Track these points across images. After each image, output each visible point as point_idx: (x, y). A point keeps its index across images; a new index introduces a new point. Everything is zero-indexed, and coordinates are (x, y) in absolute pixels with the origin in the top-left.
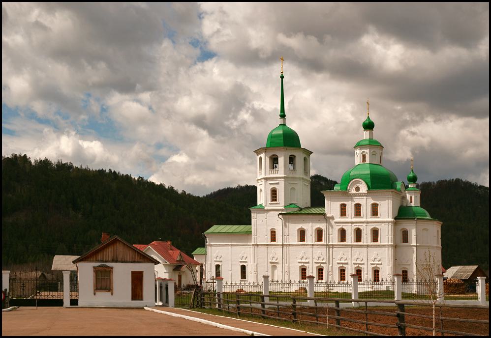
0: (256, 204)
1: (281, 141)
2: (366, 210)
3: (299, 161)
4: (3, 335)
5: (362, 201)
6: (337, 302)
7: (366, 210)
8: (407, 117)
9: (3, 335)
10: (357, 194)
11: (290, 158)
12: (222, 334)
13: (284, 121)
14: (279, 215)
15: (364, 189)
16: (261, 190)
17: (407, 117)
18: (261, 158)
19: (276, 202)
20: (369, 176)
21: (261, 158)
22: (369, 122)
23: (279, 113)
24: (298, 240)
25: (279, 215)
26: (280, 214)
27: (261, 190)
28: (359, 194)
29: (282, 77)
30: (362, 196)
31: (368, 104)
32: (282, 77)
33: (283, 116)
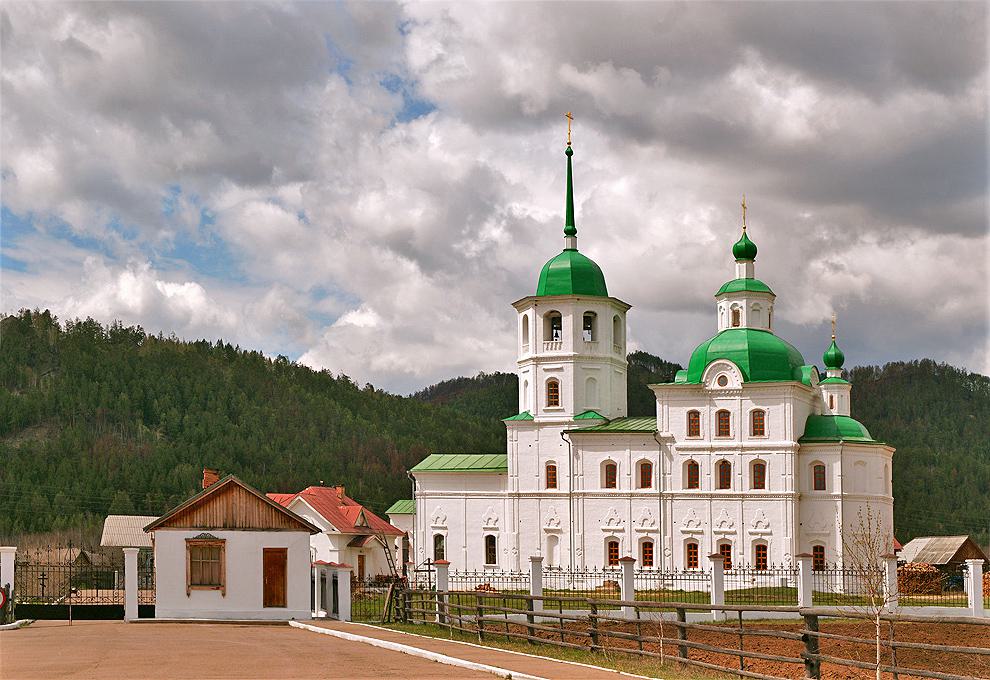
0: (517, 412)
2: (740, 423)
3: (604, 323)
7: (740, 423)
10: (721, 390)
13: (574, 243)
14: (562, 434)
15: (735, 380)
16: (526, 383)
19: (556, 408)
21: (526, 317)
24: (750, 485)
25: (562, 434)
29: (569, 153)
32: (569, 153)
33: (571, 232)
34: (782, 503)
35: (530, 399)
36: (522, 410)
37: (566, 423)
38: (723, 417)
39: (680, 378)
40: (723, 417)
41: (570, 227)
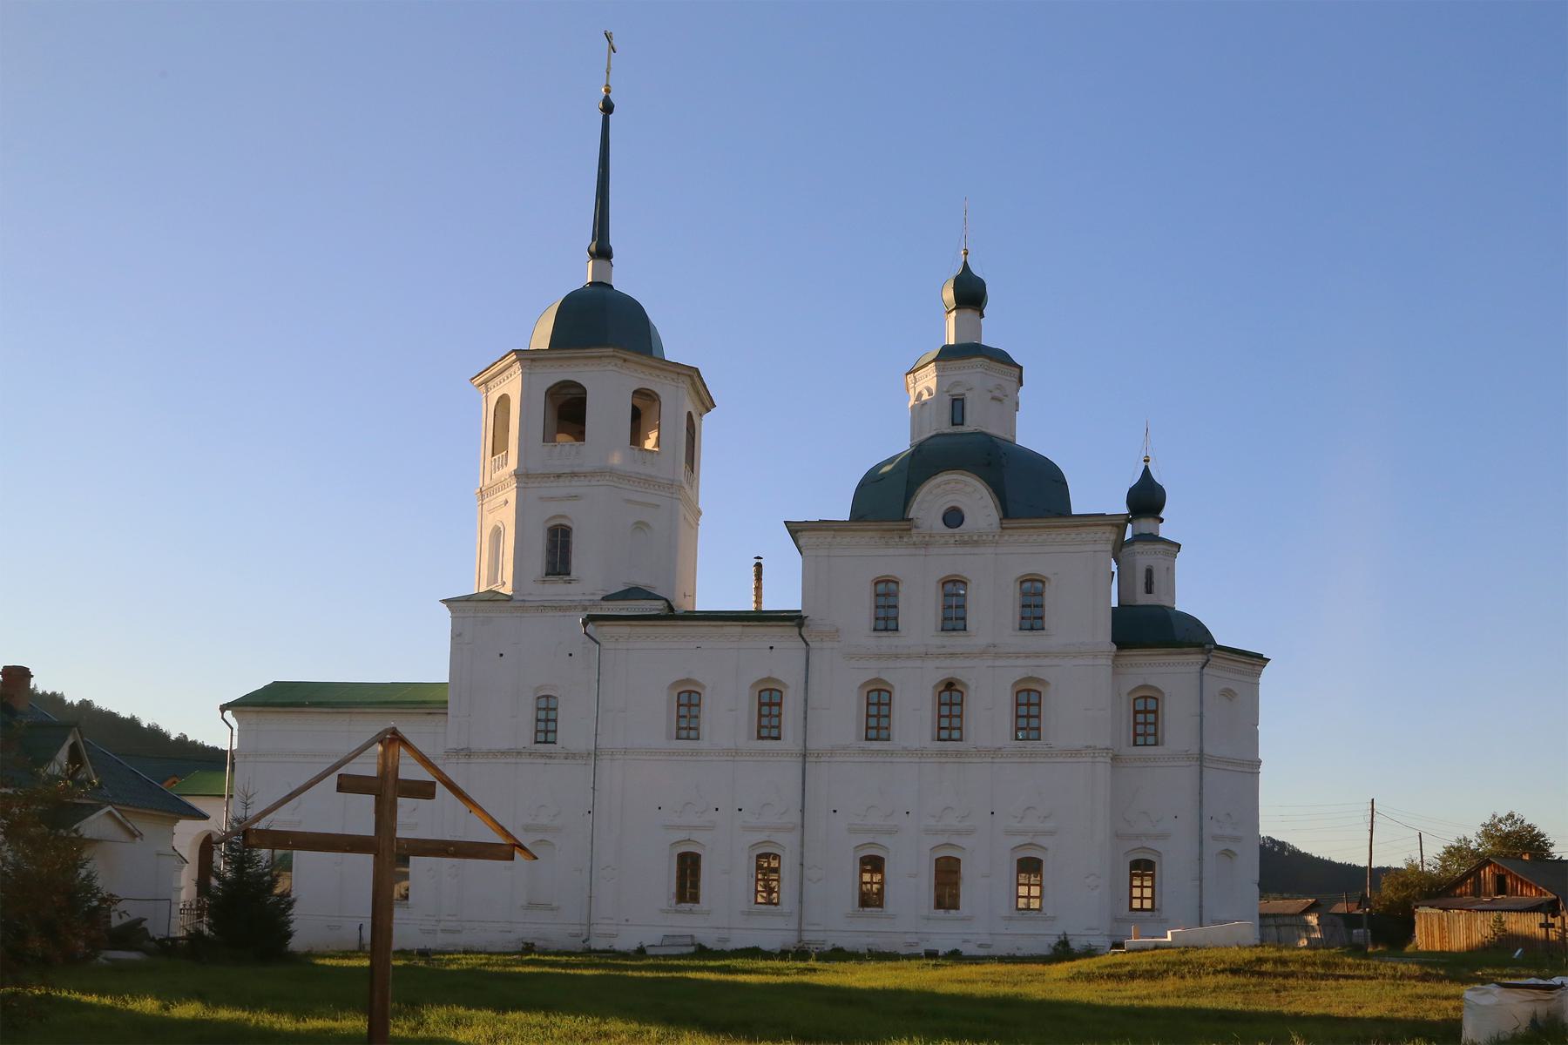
19: (567, 578)
29: (608, 108)
32: (608, 108)
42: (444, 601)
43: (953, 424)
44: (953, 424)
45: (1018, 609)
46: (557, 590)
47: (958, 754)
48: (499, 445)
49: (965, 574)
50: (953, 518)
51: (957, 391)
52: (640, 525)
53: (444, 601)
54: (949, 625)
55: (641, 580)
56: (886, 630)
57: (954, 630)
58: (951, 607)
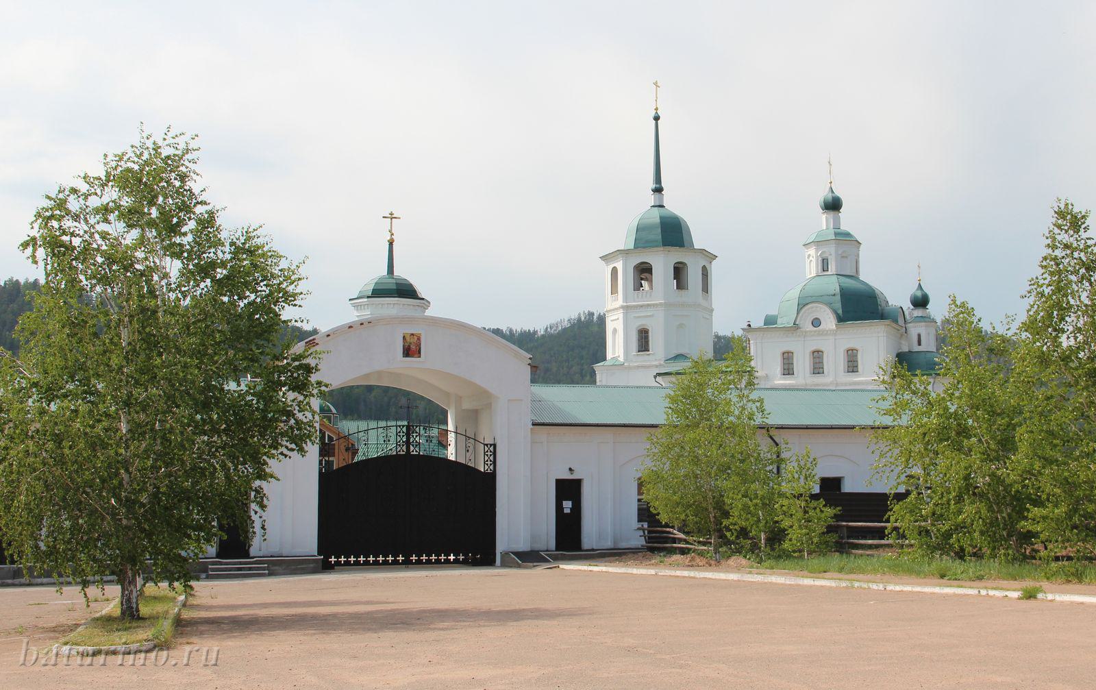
0: (604, 359)
1: (657, 235)
2: (834, 362)
3: (694, 276)
4: (571, 502)
5: (826, 345)
6: (102, 579)
7: (834, 362)
8: (435, 432)
9: (571, 502)
10: (815, 331)
11: (674, 267)
12: (288, 581)
13: (662, 199)
14: (655, 377)
15: (829, 322)
16: (615, 331)
17: (435, 432)
18: (614, 271)
19: (648, 353)
20: (838, 298)
21: (614, 271)
22: (833, 197)
23: (652, 185)
24: (844, 370)
25: (655, 377)
26: (659, 374)
27: (615, 331)
28: (819, 331)
29: (657, 118)
30: (826, 334)
31: (830, 165)
32: (657, 118)
33: (658, 190)
34: (585, 548)
35: (617, 346)
36: (609, 355)
37: (657, 366)
38: (817, 356)
39: (898, 516)
40: (817, 356)
41: (658, 186)
42: (742, 329)
43: (824, 271)
44: (824, 271)
45: (846, 363)
46: (644, 359)
47: (649, 355)
48: (614, 290)
49: (857, 347)
50: (816, 323)
51: (824, 256)
52: (681, 326)
53: (742, 329)
54: (816, 371)
55: (681, 351)
56: (789, 374)
57: (819, 373)
58: (817, 363)
